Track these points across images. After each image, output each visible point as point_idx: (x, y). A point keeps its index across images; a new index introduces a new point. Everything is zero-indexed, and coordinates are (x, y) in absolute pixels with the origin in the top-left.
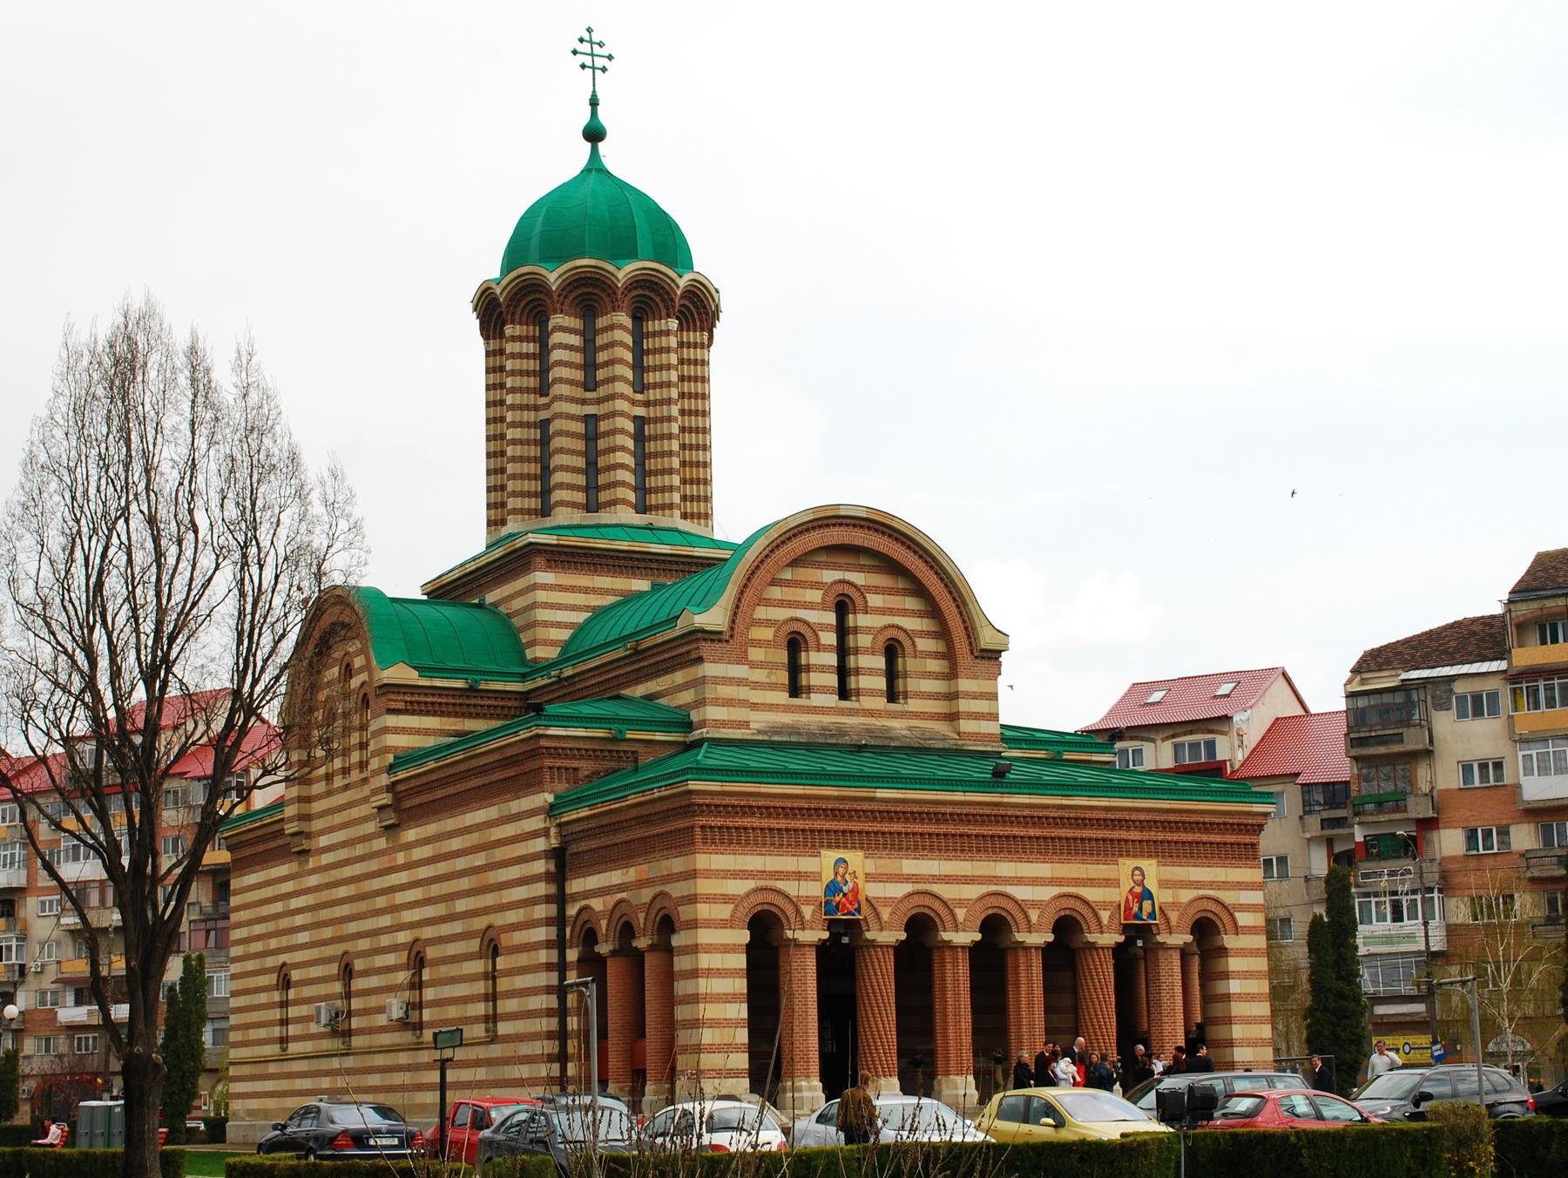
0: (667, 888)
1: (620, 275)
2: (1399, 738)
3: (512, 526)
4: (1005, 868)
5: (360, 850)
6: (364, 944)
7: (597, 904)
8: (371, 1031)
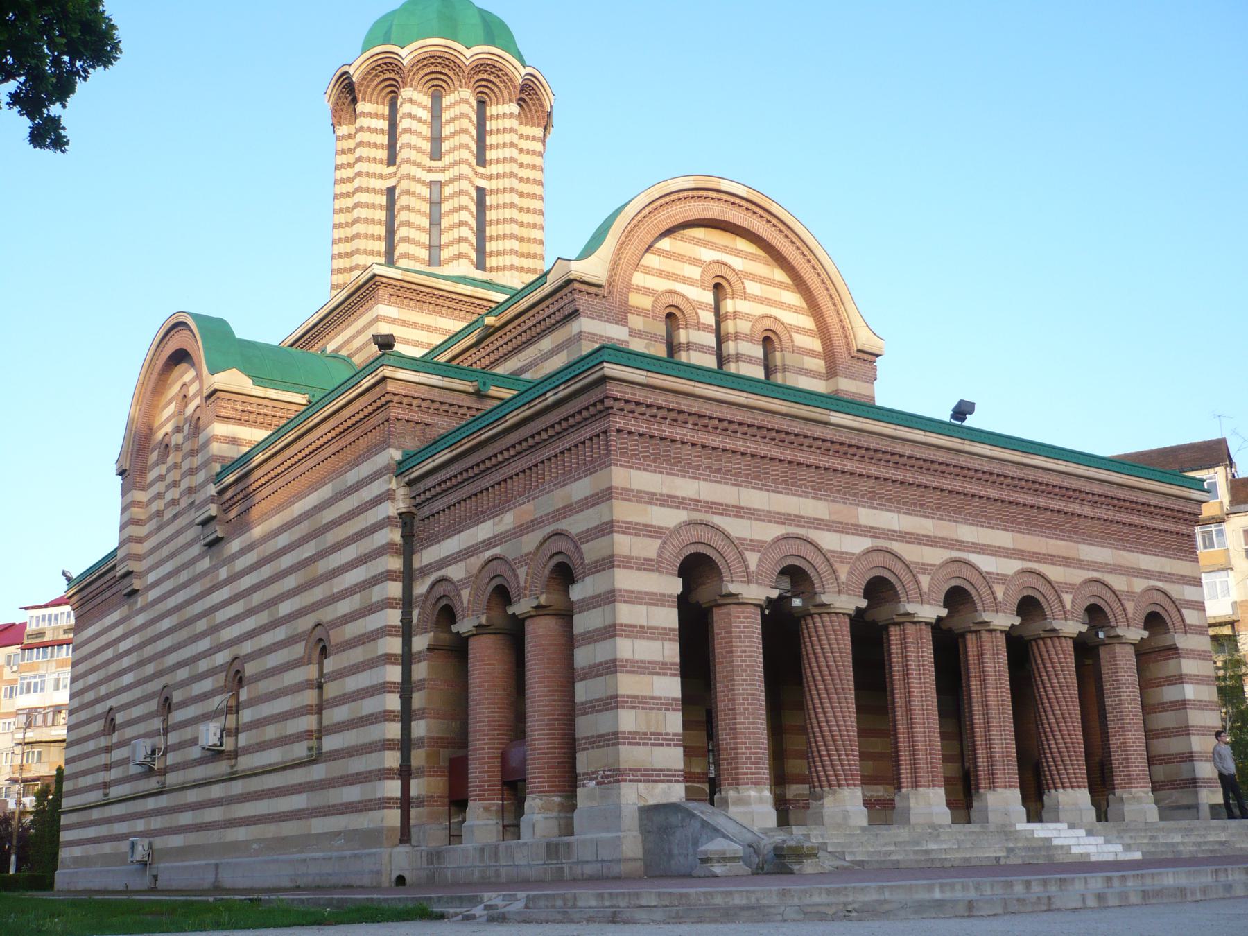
4: (967, 532)
5: (184, 576)
6: (183, 674)
7: (456, 572)
8: (185, 765)
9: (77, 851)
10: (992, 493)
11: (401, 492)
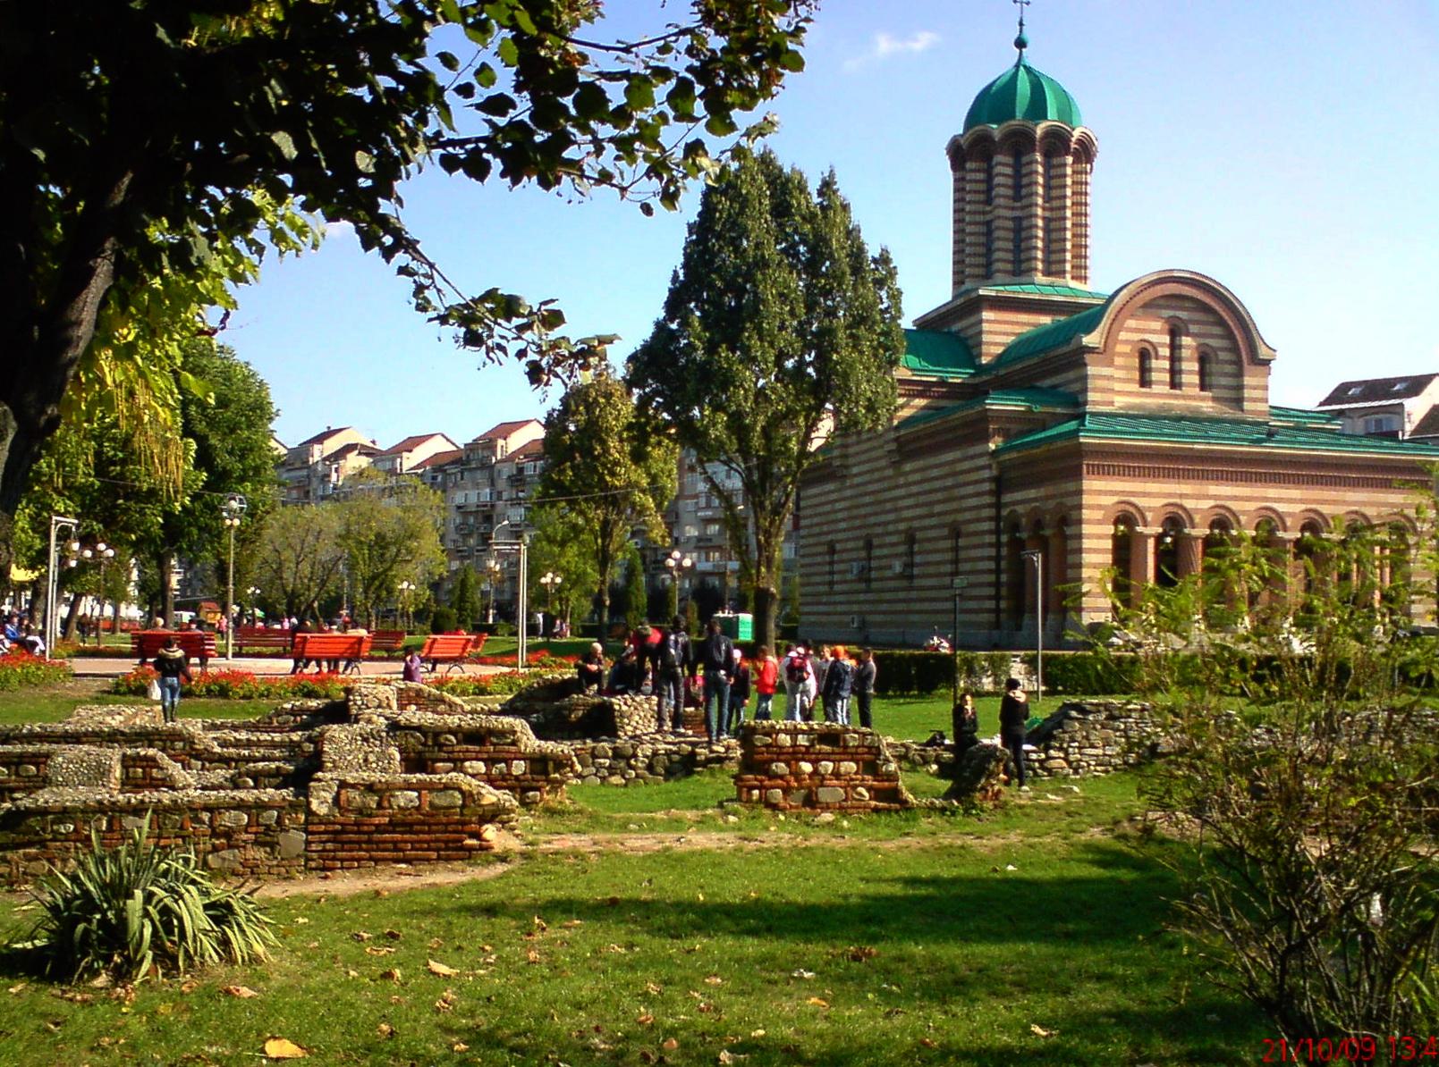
0: (1064, 500)
7: (1020, 509)
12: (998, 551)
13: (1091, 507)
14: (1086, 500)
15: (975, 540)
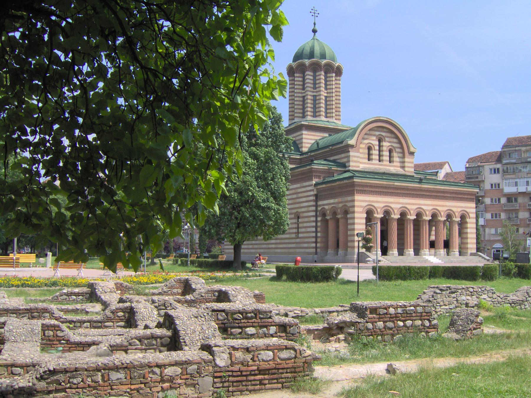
0: (347, 204)
1: (307, 63)
2: (477, 178)
3: (296, 120)
7: (326, 207)
9: (246, 251)
10: (428, 194)
11: (315, 190)
12: (316, 224)
13: (358, 206)
14: (356, 203)
15: (306, 220)
